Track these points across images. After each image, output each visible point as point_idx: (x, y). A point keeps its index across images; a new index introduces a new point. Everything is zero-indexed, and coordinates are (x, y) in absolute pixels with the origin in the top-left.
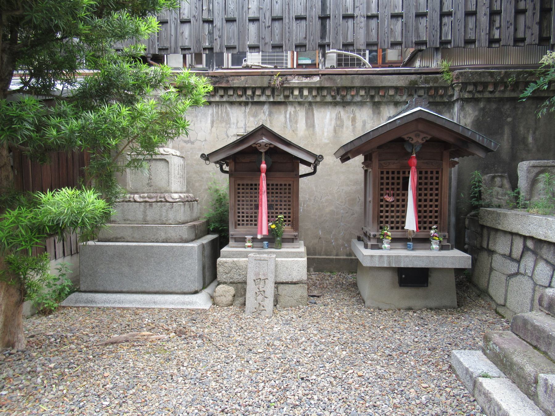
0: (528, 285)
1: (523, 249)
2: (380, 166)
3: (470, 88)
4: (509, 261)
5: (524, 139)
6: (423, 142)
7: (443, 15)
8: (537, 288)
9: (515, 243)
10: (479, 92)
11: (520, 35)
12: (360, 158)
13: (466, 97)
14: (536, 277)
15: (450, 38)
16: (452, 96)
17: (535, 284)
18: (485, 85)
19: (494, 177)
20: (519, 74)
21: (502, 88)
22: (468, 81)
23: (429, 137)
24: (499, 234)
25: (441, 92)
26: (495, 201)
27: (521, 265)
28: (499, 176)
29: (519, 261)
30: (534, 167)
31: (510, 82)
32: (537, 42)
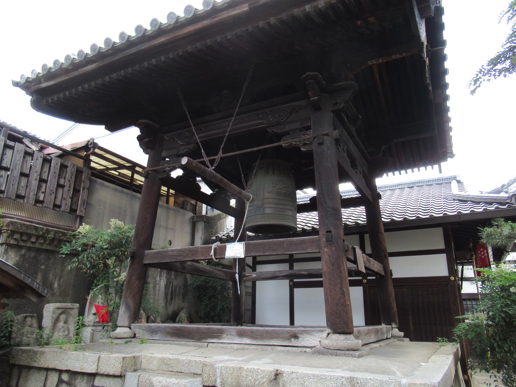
1: (58, 382)
3: (17, 236)
5: (52, 284)
7: (23, 174)
10: (24, 241)
11: (58, 202)
13: (12, 243)
15: (3, 189)
18: (30, 236)
19: (26, 317)
20: (56, 232)
21: (42, 241)
22: (16, 230)
24: (32, 371)
26: (25, 339)
28: (30, 316)
30: (58, 308)
31: (49, 237)
32: (68, 211)
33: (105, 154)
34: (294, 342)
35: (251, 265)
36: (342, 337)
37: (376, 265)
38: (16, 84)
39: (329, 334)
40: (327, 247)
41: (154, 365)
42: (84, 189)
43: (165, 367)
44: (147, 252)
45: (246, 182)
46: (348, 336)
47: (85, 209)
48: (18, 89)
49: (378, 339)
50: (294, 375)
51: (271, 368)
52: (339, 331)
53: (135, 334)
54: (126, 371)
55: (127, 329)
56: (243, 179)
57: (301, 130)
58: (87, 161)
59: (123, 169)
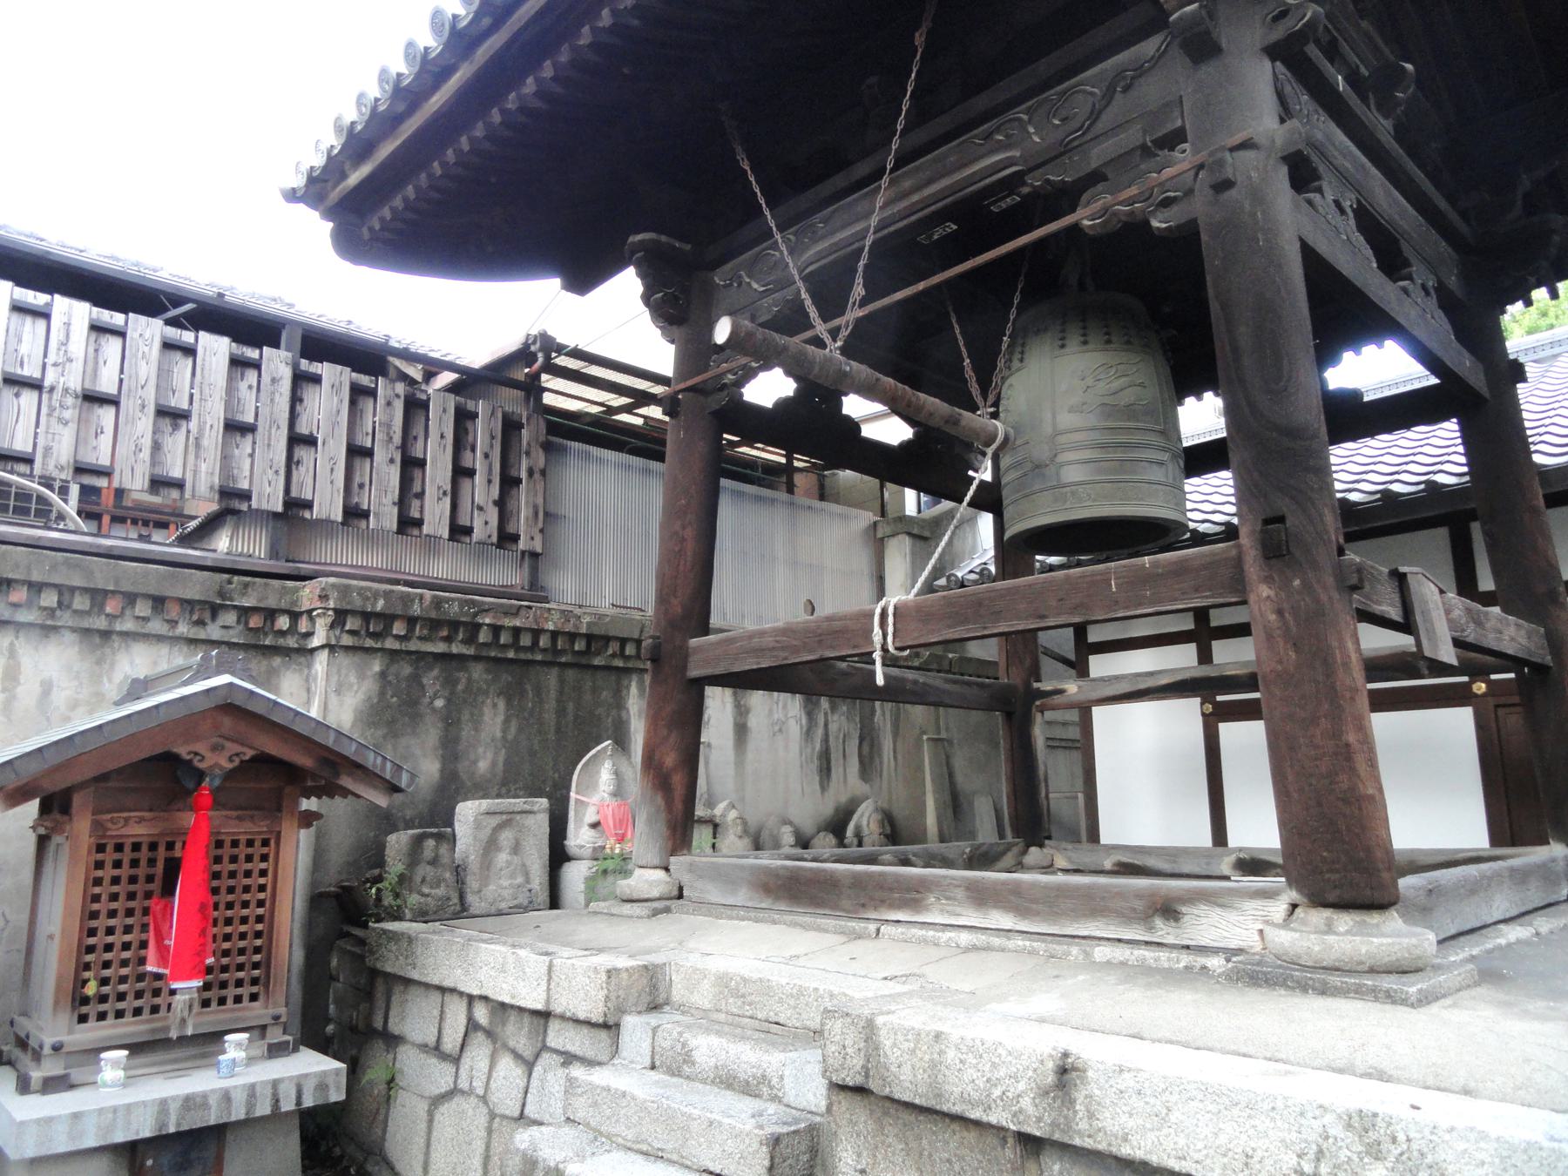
0: (477, 1118)
2: (97, 826)
4: (434, 1061)
6: (230, 766)
8: (495, 1125)
9: (449, 1015)
12: (33, 807)
14: (494, 1098)
16: (309, 635)
17: (492, 1116)
23: (249, 754)
24: (414, 990)
25: (283, 622)
27: (462, 1070)
29: (456, 1060)
32: (494, 539)
33: (586, 366)
34: (1164, 931)
35: (1072, 656)
36: (1345, 921)
37: (1511, 631)
38: (292, 196)
39: (1294, 906)
40: (1268, 580)
41: (703, 997)
42: (531, 473)
43: (733, 1005)
44: (694, 642)
45: (985, 388)
46: (1374, 918)
47: (541, 531)
48: (302, 208)
49: (1523, 909)
50: (1127, 1081)
51: (1045, 1044)
52: (1331, 897)
53: (681, 889)
54: (622, 1011)
55: (661, 874)
56: (969, 373)
57: (1146, 151)
58: (533, 389)
59: (648, 405)
